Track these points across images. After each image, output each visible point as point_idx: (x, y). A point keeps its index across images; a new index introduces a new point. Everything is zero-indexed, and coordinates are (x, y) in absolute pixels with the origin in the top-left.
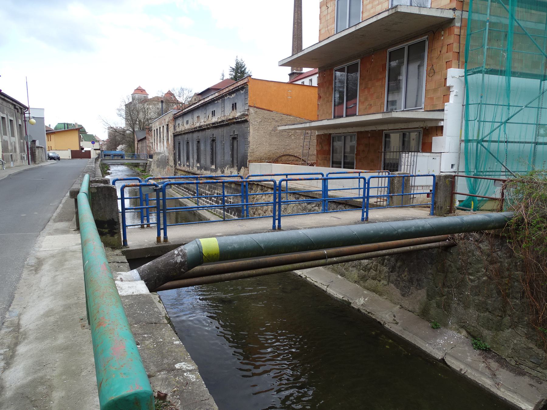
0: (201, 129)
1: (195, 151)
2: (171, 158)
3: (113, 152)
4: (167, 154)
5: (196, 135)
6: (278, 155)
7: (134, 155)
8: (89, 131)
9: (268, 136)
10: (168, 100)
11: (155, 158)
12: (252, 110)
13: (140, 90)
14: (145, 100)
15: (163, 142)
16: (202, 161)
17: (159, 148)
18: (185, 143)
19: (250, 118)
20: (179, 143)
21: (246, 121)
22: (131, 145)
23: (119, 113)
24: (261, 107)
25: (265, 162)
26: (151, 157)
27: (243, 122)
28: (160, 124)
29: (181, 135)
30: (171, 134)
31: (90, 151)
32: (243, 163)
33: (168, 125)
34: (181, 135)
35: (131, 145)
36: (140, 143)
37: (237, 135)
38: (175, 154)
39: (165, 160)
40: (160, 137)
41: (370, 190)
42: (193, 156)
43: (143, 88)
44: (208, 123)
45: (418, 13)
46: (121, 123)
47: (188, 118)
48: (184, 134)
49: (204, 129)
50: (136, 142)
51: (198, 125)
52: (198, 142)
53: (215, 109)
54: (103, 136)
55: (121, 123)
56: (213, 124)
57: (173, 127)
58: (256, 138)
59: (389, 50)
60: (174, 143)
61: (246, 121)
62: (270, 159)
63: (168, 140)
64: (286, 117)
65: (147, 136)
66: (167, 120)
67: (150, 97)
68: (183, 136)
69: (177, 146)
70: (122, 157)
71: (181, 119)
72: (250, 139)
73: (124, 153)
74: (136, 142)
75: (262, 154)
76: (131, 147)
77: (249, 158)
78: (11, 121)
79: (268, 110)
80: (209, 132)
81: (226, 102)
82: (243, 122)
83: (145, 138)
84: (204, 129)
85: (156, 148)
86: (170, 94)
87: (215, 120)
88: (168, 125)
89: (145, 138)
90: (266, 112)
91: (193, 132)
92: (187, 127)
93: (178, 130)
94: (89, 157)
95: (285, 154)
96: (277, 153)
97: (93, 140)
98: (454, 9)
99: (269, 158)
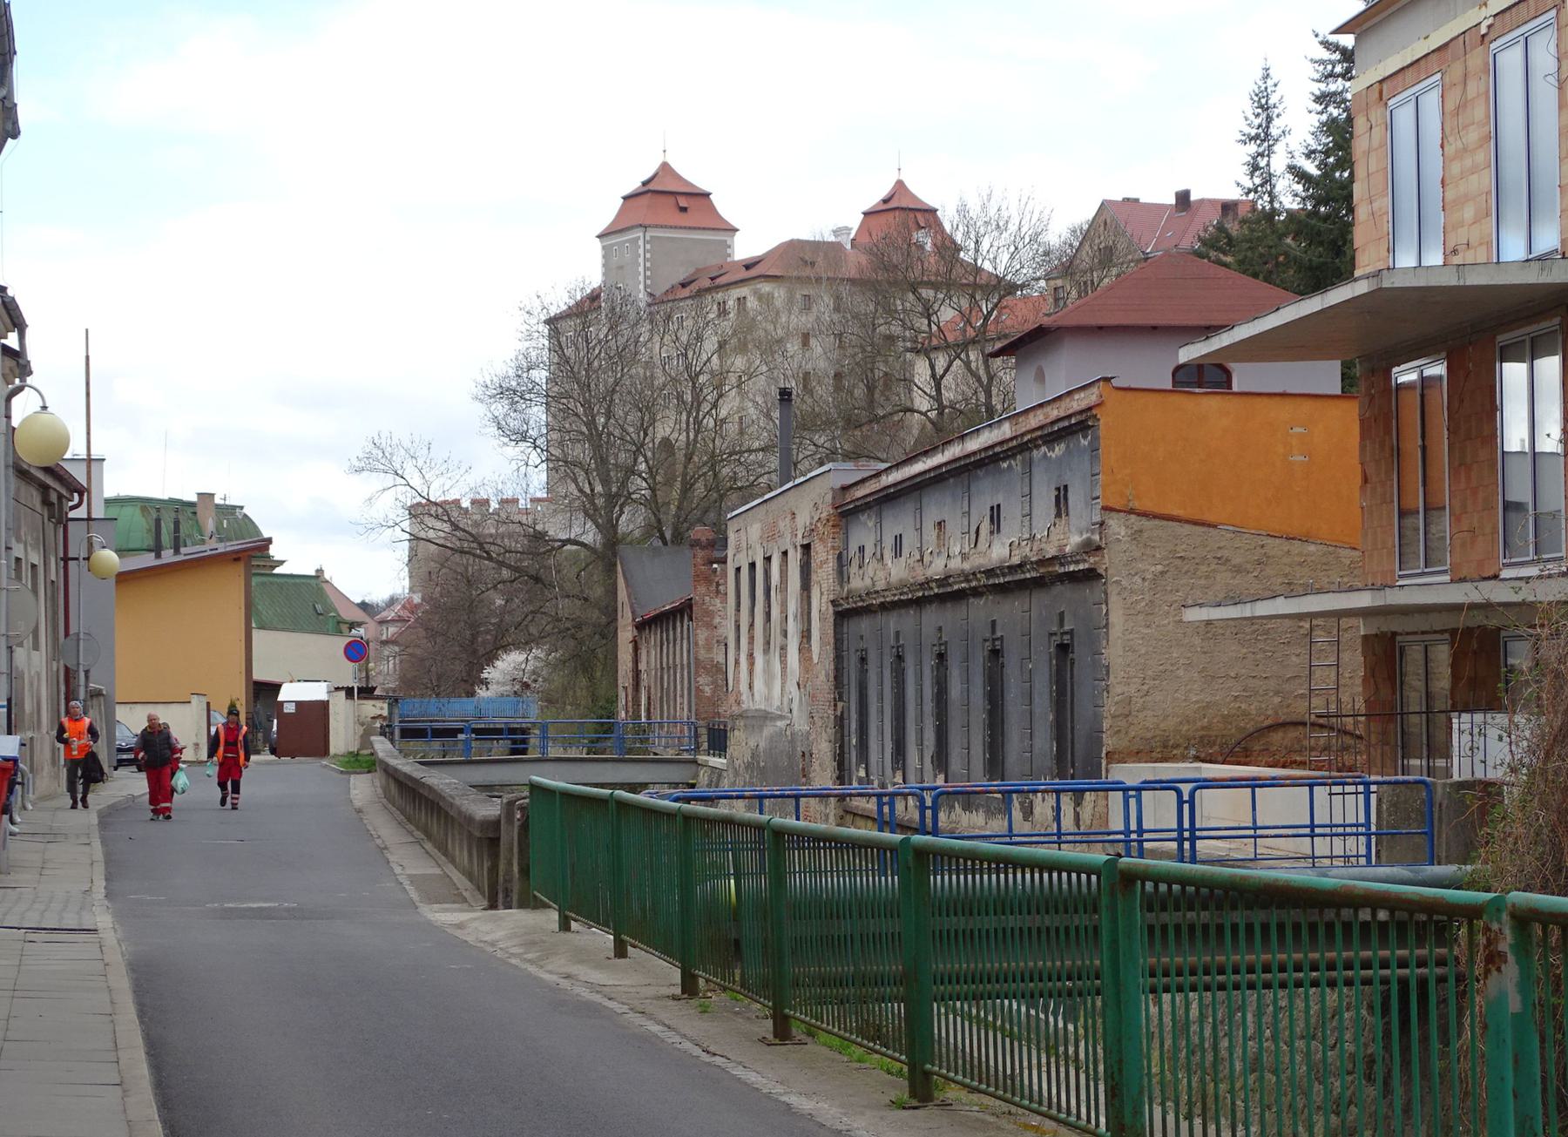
0: (948, 594)
1: (929, 706)
2: (823, 749)
3: (455, 710)
4: (801, 724)
5: (932, 618)
6: (1250, 727)
7: (609, 729)
8: (294, 556)
9: (1197, 641)
10: (903, 251)
11: (742, 743)
12: (1118, 527)
13: (667, 202)
14: (710, 282)
15: (783, 648)
16: (956, 763)
18: (888, 660)
19: (1109, 562)
20: (863, 660)
22: (587, 653)
24: (1157, 510)
25: (1184, 758)
26: (718, 742)
28: (771, 535)
29: (868, 610)
30: (820, 603)
31: (322, 707)
32: (1076, 761)
33: (807, 548)
34: (868, 610)
35: (587, 653)
36: (654, 637)
37: (1071, 632)
38: (840, 722)
39: (791, 757)
40: (768, 615)
41: (1259, 824)
42: (921, 732)
45: (1454, 282)
46: (502, 471)
48: (884, 607)
49: (960, 596)
50: (626, 634)
51: (937, 567)
53: (999, 499)
54: (374, 572)
55: (502, 471)
56: (990, 573)
57: (831, 565)
58: (1148, 651)
59: (1500, 338)
60: (839, 658)
61: (1091, 576)
62: (1211, 744)
63: (806, 635)
64: (1286, 545)
65: (699, 593)
66: (803, 519)
67: (744, 248)
68: (880, 619)
69: (847, 676)
70: (517, 741)
71: (868, 520)
72: (1114, 653)
73: (533, 711)
74: (626, 634)
75: (1171, 723)
77: (1109, 742)
78: (34, 566)
79: (1196, 523)
80: (980, 610)
83: (684, 610)
84: (960, 596)
85: (744, 687)
86: (901, 214)
87: (998, 552)
88: (807, 548)
90: (1188, 528)
91: (919, 603)
93: (857, 583)
94: (320, 748)
95: (1283, 718)
96: (1246, 714)
99: (1205, 741)
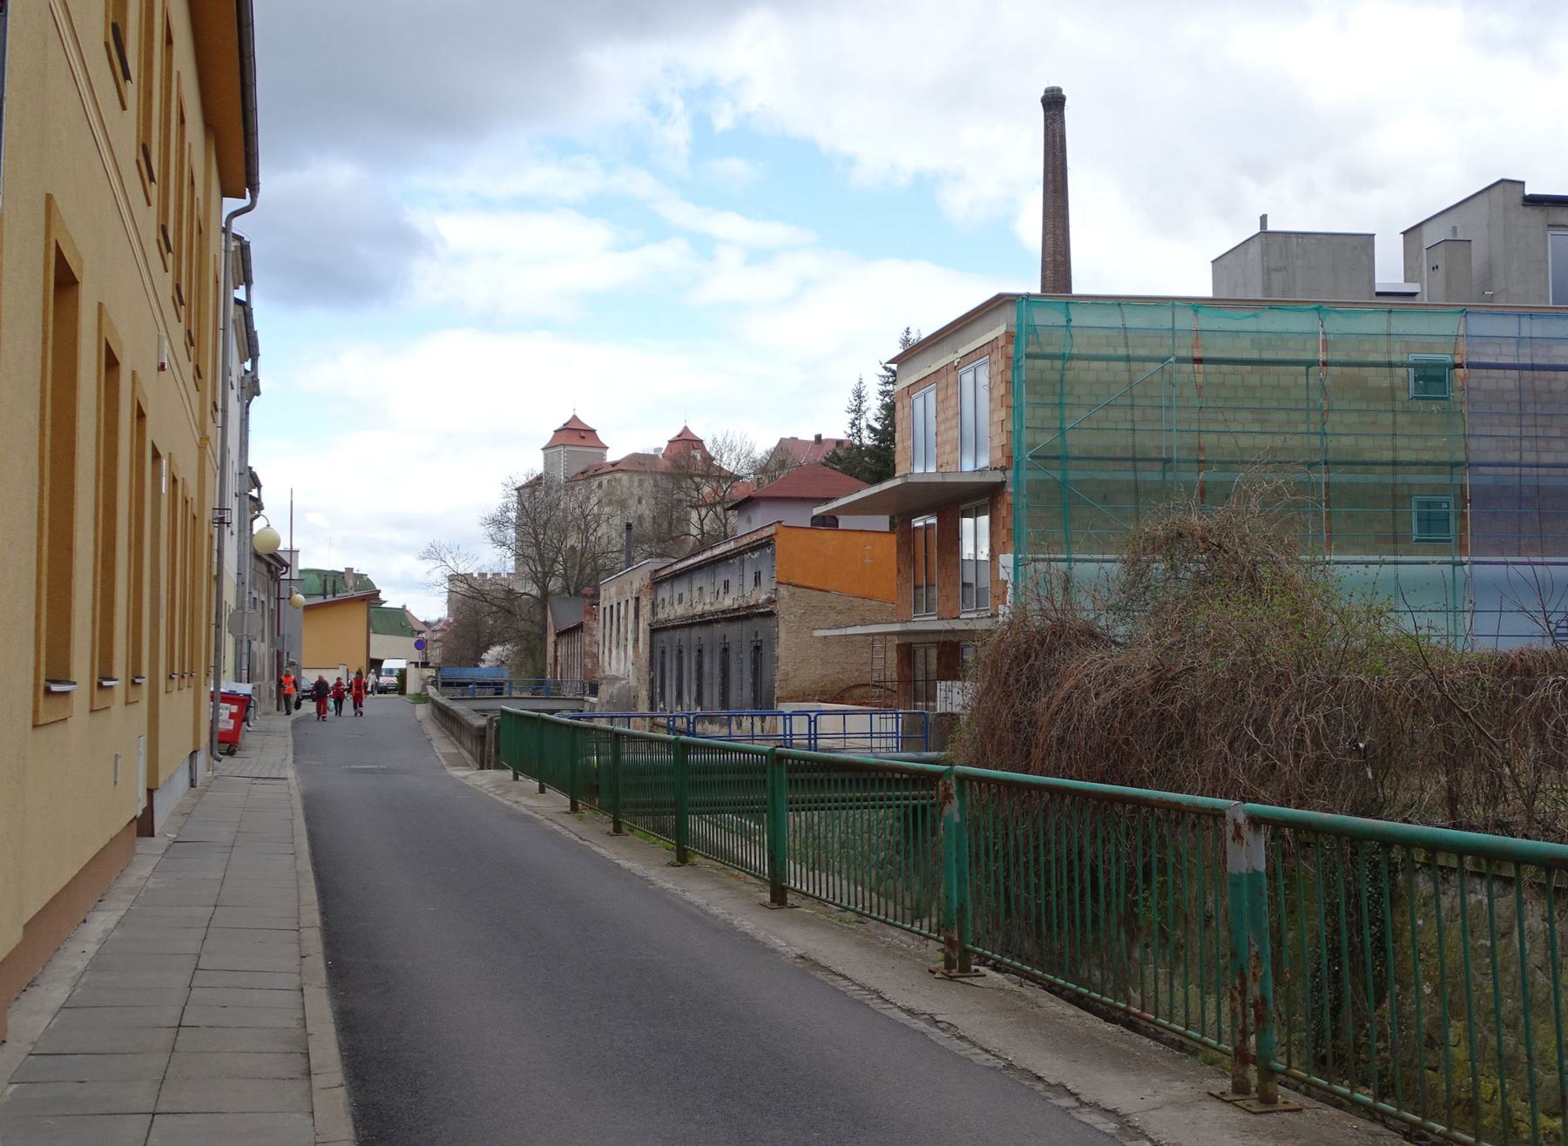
0: (704, 621)
2: (644, 694)
4: (633, 683)
5: (696, 633)
7: (542, 683)
11: (604, 691)
12: (783, 591)
13: (575, 434)
16: (706, 702)
17: (614, 663)
18: (694, 654)
19: (779, 608)
21: (771, 614)
22: (532, 648)
23: (500, 537)
26: (594, 690)
27: (766, 614)
28: (620, 593)
29: (666, 629)
30: (643, 625)
32: (762, 702)
33: (637, 599)
34: (666, 629)
35: (532, 648)
38: (652, 682)
43: (588, 420)
44: (717, 606)
46: (494, 560)
47: (681, 587)
49: (710, 622)
50: (551, 638)
51: (699, 609)
52: (700, 651)
53: (728, 577)
54: (431, 607)
55: (494, 560)
56: (723, 612)
57: (649, 607)
58: (797, 650)
60: (652, 652)
61: (771, 614)
63: (636, 640)
65: (587, 620)
66: (636, 585)
67: (612, 456)
69: (656, 660)
70: (498, 688)
71: (667, 586)
72: (780, 651)
73: (505, 675)
74: (551, 638)
76: (533, 655)
81: (747, 566)
82: (766, 614)
83: (579, 627)
84: (710, 622)
86: (686, 443)
87: (728, 602)
88: (637, 599)
89: (579, 627)
91: (690, 626)
92: (680, 610)
93: (661, 616)
97: (399, 621)
98: (1003, 469)
99: (823, 693)
